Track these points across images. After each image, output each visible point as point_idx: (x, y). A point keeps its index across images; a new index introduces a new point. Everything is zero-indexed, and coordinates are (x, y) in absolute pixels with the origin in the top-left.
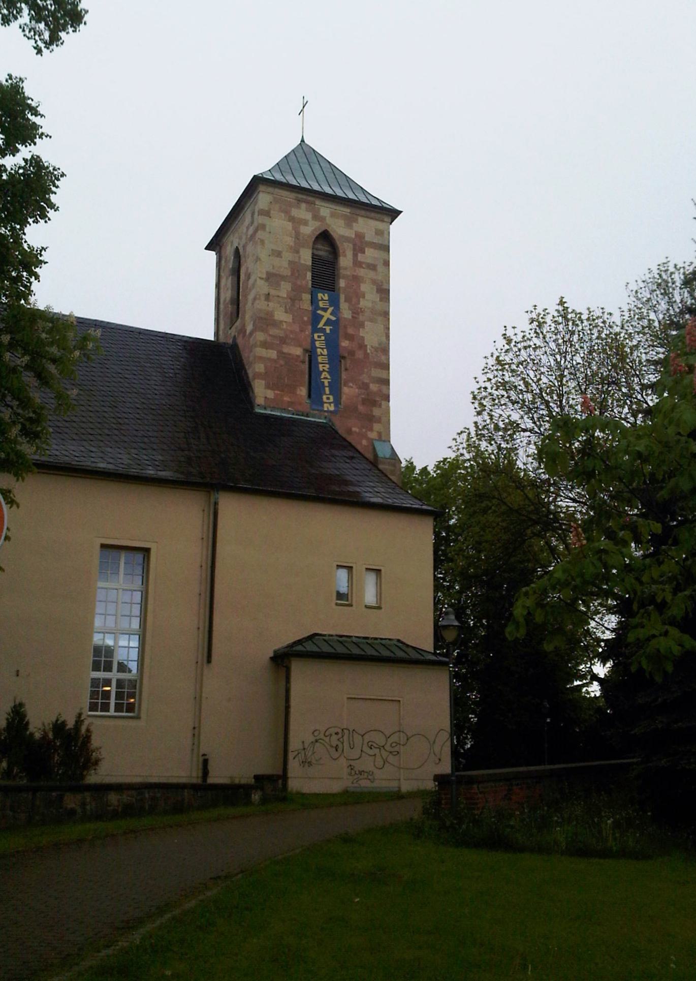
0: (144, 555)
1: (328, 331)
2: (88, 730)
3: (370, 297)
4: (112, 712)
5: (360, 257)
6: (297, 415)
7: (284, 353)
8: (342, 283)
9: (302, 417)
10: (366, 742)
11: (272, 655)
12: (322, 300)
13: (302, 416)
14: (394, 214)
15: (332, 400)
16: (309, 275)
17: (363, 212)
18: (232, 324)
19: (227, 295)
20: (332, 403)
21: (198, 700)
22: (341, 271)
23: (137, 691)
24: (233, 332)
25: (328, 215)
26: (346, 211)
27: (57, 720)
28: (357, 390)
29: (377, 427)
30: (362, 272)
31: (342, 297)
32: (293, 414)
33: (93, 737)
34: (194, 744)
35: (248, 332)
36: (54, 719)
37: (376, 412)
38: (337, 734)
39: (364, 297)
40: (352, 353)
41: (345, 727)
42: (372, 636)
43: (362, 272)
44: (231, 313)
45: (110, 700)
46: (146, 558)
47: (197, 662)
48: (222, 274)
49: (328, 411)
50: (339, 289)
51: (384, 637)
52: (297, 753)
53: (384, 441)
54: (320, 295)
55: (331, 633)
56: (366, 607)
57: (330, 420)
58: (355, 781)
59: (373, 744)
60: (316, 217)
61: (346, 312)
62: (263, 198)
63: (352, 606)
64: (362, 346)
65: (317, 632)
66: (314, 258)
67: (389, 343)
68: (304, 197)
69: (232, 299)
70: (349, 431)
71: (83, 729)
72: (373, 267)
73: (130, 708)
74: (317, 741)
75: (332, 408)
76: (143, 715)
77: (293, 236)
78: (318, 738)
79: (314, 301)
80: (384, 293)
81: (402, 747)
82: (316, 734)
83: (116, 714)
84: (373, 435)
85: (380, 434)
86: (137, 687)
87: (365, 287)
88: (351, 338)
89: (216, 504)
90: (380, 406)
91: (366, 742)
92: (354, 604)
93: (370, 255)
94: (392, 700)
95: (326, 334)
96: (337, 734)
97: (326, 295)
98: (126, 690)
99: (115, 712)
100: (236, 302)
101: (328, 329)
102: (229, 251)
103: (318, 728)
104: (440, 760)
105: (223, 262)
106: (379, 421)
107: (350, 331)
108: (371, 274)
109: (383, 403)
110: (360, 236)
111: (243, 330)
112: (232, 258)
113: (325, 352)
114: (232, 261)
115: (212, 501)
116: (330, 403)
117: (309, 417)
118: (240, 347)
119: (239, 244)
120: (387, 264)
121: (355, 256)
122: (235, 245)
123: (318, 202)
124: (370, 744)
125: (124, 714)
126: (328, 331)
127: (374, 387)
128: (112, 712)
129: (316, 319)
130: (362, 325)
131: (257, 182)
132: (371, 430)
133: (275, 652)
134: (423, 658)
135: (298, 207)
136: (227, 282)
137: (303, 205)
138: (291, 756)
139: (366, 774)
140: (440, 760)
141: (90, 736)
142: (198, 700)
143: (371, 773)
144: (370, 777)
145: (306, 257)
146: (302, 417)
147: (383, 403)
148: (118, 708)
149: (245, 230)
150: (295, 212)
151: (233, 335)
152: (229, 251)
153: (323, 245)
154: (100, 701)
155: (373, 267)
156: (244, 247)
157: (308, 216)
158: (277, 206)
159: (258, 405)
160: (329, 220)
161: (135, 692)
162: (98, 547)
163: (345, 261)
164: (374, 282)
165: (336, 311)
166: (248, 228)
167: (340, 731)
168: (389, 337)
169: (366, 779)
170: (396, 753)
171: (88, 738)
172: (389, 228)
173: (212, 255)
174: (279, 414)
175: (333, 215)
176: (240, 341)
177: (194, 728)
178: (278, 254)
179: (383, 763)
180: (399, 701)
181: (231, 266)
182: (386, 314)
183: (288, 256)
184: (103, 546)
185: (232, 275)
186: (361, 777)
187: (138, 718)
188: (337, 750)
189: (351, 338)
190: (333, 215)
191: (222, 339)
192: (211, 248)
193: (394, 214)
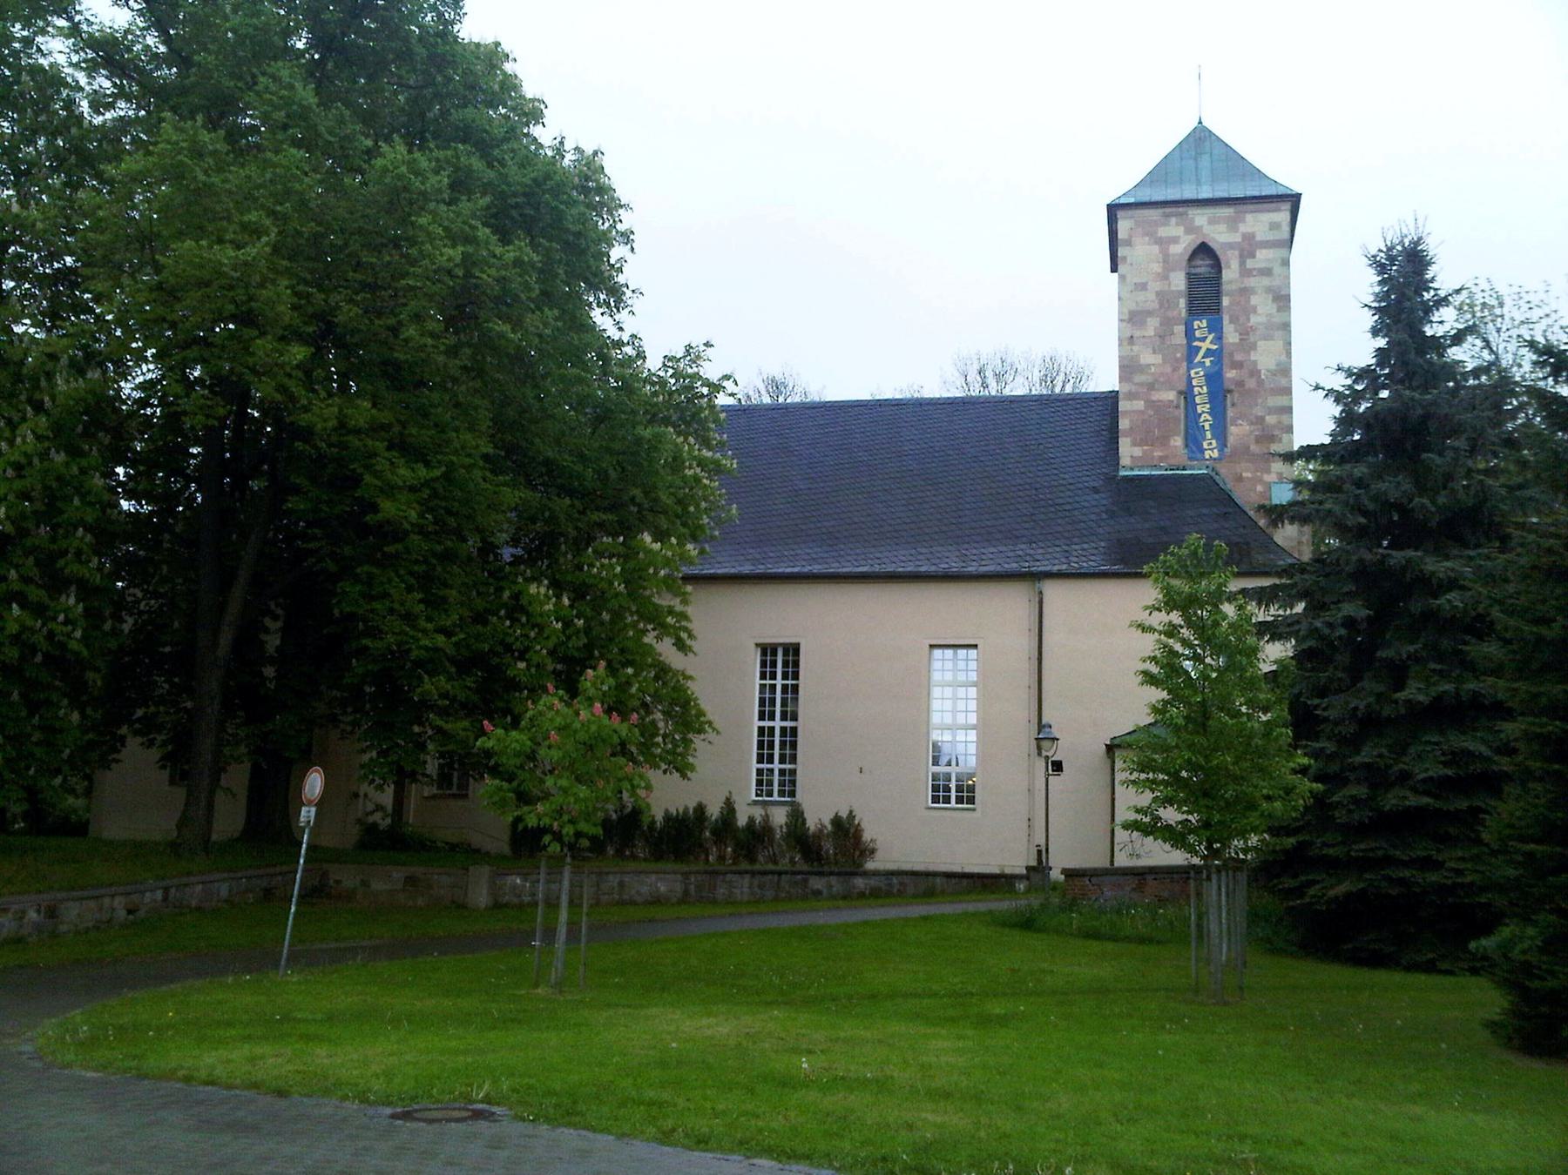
3: (1263, 308)
5: (1250, 264)
8: (1226, 301)
43: (1251, 282)
61: (1231, 335)
72: (1267, 272)
80: (1282, 300)
83: (960, 806)
88: (1238, 365)
99: (957, 803)
108: (1266, 281)
116: (1212, 450)
125: (965, 806)
135: (1165, 224)
145: (1179, 281)
148: (959, 800)
155: (1267, 272)
164: (1269, 290)
175: (1212, 221)
182: (1286, 327)
189: (1238, 365)
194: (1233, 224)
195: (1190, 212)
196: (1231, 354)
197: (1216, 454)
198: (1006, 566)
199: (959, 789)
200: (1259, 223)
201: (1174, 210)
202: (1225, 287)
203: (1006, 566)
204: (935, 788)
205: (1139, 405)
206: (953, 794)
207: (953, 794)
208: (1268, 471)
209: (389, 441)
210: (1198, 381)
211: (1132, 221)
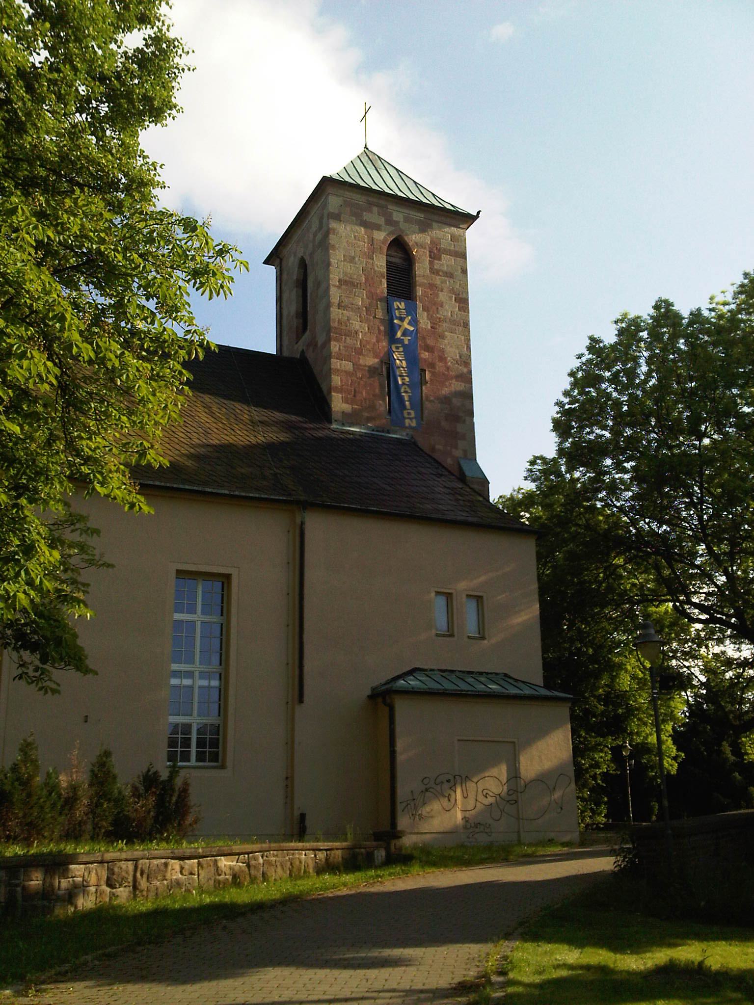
0: (223, 583)
1: (406, 342)
2: (186, 784)
3: (449, 308)
4: (193, 761)
5: (437, 265)
6: (377, 431)
7: (361, 365)
8: (419, 291)
9: (383, 434)
10: (480, 790)
11: (369, 692)
12: (399, 308)
13: (383, 432)
14: (469, 219)
15: (413, 415)
16: (384, 281)
17: (436, 218)
18: (298, 338)
19: (292, 308)
20: (413, 418)
21: (290, 744)
22: (417, 279)
23: (221, 737)
24: (301, 346)
25: (402, 220)
26: (420, 216)
27: (149, 771)
28: (439, 405)
29: (461, 444)
30: (438, 280)
31: (419, 305)
32: (373, 430)
33: (191, 790)
34: (287, 797)
35: (319, 344)
36: (145, 770)
37: (460, 428)
38: (448, 781)
39: (442, 306)
40: (432, 365)
41: (457, 774)
42: (477, 670)
43: (438, 280)
44: (297, 327)
45: (190, 748)
46: (225, 585)
47: (287, 703)
48: (284, 288)
49: (410, 427)
50: (416, 297)
51: (490, 671)
52: (405, 804)
53: (470, 460)
54: (396, 304)
55: (432, 667)
56: (469, 637)
57: (412, 438)
58: (471, 836)
59: (489, 792)
60: (390, 222)
61: (424, 322)
62: (334, 202)
63: (454, 636)
64: (442, 359)
65: (417, 667)
66: (389, 265)
67: (470, 356)
68: (375, 200)
69: (297, 313)
70: (433, 449)
71: (178, 782)
72: (450, 275)
73: (215, 757)
74: (427, 790)
75: (414, 424)
76: (229, 763)
77: (366, 241)
78: (428, 786)
79: (389, 310)
80: (463, 302)
81: (519, 794)
82: (426, 781)
83: (201, 764)
84: (458, 453)
85: (465, 451)
86: (221, 733)
87: (443, 297)
88: (428, 348)
89: (302, 523)
90: (464, 421)
91: (480, 790)
92: (456, 633)
93: (447, 262)
94: (473, 741)
95: (404, 346)
96: (448, 781)
97: (403, 304)
98: (180, 736)
99: (197, 761)
100: (303, 315)
101: (406, 340)
102: (292, 262)
103: (425, 776)
104: (562, 809)
105: (285, 276)
106: (463, 437)
107: (430, 342)
108: (449, 282)
109: (467, 418)
110: (435, 243)
111: (313, 344)
112: (296, 269)
113: (404, 364)
114: (296, 272)
115: (298, 521)
116: (411, 419)
117: (389, 433)
118: (310, 360)
119: (305, 253)
120: (465, 272)
121: (431, 263)
122: (300, 255)
123: (391, 207)
124: (485, 792)
125: (207, 764)
126: (406, 342)
127: (456, 402)
128: (193, 761)
129: (391, 329)
130: (442, 337)
131: (326, 183)
132: (456, 448)
133: (373, 689)
134: (521, 692)
135: (371, 211)
136: (292, 295)
137: (375, 209)
138: (399, 807)
139: (482, 827)
140: (562, 809)
141: (188, 790)
142: (290, 744)
143: (488, 826)
144: (488, 830)
145: (380, 263)
146: (383, 434)
147: (467, 418)
148: (200, 757)
149: (311, 236)
150: (367, 216)
151: (300, 349)
152: (292, 262)
153: (396, 251)
154: (179, 750)
155: (450, 275)
156: (311, 255)
157: (381, 221)
158: (348, 209)
159: (336, 421)
160: (402, 225)
161: (218, 739)
162: (174, 574)
163: (422, 269)
164: (452, 291)
165: (414, 322)
166: (315, 235)
167: (451, 778)
168: (470, 349)
169: (482, 832)
170: (465, 796)
171: (184, 791)
172: (464, 235)
173: (272, 270)
174: (358, 430)
175: (407, 220)
176: (310, 356)
177: (287, 778)
178: (352, 260)
179: (500, 813)
180: (514, 743)
181: (295, 277)
182: (466, 325)
183: (361, 262)
184: (179, 572)
185: (297, 287)
186: (477, 830)
187: (223, 767)
188: (449, 800)
189: (428, 348)
190: (407, 220)
191: (286, 353)
192: (270, 263)
193: (469, 219)
194: (424, 228)
195: (390, 207)
196: (424, 338)
197: (414, 424)
198: (211, 441)
199: (201, 743)
200: (444, 233)
201: (299, 232)
202: (419, 280)
203: (211, 441)
204: (172, 743)
205: (348, 366)
206: (194, 749)
207: (194, 749)
208: (456, 447)
209: (665, 345)
210: (399, 359)
211: (341, 199)
